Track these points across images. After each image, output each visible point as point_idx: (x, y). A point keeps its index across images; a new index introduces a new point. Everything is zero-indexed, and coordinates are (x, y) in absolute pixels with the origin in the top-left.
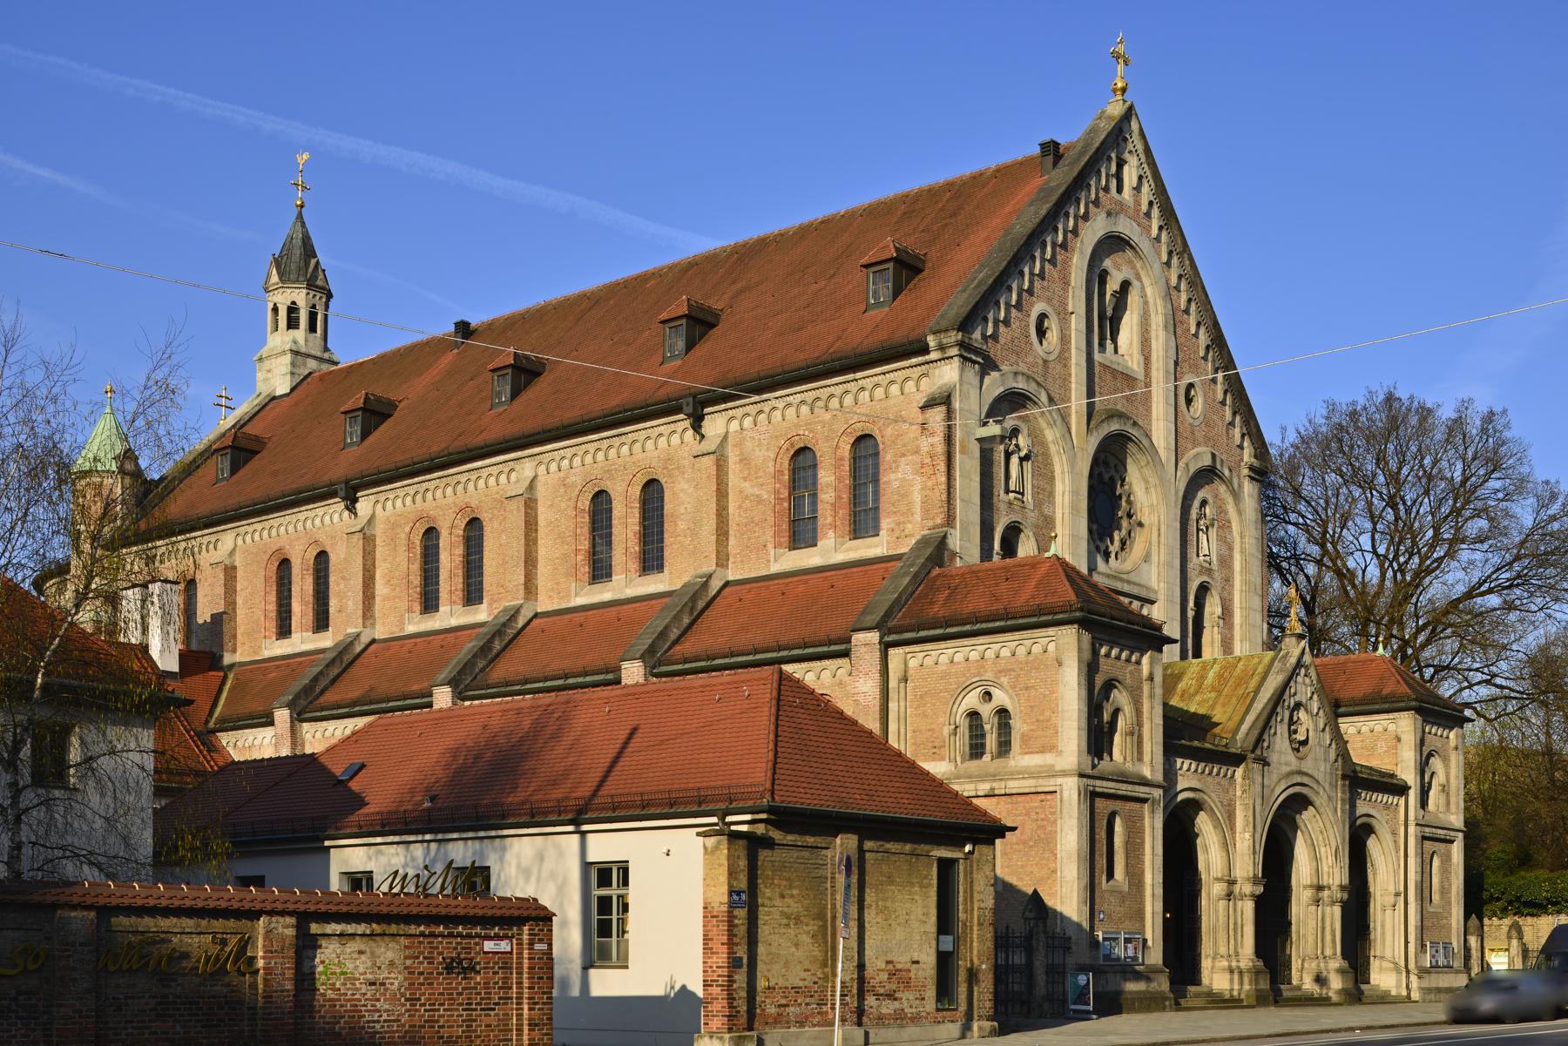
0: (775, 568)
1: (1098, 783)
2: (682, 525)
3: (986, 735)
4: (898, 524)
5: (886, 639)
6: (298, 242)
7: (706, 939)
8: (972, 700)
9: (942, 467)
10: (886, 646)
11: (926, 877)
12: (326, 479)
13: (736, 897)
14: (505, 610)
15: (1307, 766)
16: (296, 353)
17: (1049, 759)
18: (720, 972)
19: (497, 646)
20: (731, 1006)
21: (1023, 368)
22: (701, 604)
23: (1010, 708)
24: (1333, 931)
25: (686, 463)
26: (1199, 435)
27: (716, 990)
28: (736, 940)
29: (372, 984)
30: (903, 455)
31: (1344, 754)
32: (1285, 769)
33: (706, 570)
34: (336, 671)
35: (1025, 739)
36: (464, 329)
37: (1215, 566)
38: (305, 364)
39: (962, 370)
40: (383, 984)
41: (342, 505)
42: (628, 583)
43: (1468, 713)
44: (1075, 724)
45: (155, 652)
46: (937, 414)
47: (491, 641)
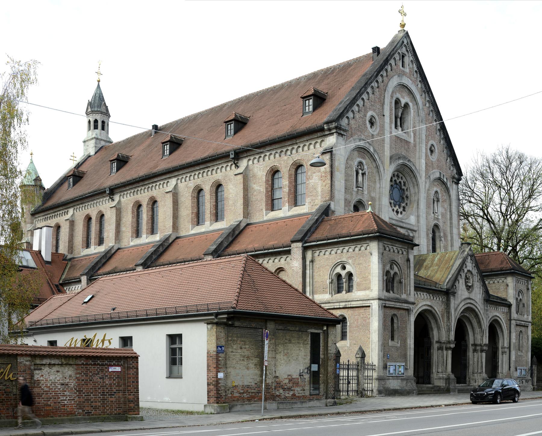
0: (265, 218)
1: (387, 302)
2: (231, 202)
3: (342, 282)
7: (208, 366)
8: (338, 270)
9: (329, 177)
10: (305, 249)
11: (306, 340)
12: (102, 187)
13: (220, 349)
14: (165, 236)
15: (472, 296)
16: (97, 139)
17: (367, 292)
18: (213, 379)
19: (161, 250)
20: (218, 393)
21: (363, 137)
22: (237, 232)
23: (352, 272)
24: (482, 363)
25: (232, 177)
26: (435, 166)
27: (212, 387)
28: (219, 366)
29: (62, 384)
30: (314, 173)
31: (486, 291)
32: (464, 297)
34: (104, 261)
35: (358, 284)
36: (155, 127)
37: (440, 217)
38: (100, 143)
39: (337, 139)
40: (68, 385)
41: (108, 198)
42: (211, 224)
43: (533, 275)
44: (377, 279)
45: (43, 254)
47: (158, 248)
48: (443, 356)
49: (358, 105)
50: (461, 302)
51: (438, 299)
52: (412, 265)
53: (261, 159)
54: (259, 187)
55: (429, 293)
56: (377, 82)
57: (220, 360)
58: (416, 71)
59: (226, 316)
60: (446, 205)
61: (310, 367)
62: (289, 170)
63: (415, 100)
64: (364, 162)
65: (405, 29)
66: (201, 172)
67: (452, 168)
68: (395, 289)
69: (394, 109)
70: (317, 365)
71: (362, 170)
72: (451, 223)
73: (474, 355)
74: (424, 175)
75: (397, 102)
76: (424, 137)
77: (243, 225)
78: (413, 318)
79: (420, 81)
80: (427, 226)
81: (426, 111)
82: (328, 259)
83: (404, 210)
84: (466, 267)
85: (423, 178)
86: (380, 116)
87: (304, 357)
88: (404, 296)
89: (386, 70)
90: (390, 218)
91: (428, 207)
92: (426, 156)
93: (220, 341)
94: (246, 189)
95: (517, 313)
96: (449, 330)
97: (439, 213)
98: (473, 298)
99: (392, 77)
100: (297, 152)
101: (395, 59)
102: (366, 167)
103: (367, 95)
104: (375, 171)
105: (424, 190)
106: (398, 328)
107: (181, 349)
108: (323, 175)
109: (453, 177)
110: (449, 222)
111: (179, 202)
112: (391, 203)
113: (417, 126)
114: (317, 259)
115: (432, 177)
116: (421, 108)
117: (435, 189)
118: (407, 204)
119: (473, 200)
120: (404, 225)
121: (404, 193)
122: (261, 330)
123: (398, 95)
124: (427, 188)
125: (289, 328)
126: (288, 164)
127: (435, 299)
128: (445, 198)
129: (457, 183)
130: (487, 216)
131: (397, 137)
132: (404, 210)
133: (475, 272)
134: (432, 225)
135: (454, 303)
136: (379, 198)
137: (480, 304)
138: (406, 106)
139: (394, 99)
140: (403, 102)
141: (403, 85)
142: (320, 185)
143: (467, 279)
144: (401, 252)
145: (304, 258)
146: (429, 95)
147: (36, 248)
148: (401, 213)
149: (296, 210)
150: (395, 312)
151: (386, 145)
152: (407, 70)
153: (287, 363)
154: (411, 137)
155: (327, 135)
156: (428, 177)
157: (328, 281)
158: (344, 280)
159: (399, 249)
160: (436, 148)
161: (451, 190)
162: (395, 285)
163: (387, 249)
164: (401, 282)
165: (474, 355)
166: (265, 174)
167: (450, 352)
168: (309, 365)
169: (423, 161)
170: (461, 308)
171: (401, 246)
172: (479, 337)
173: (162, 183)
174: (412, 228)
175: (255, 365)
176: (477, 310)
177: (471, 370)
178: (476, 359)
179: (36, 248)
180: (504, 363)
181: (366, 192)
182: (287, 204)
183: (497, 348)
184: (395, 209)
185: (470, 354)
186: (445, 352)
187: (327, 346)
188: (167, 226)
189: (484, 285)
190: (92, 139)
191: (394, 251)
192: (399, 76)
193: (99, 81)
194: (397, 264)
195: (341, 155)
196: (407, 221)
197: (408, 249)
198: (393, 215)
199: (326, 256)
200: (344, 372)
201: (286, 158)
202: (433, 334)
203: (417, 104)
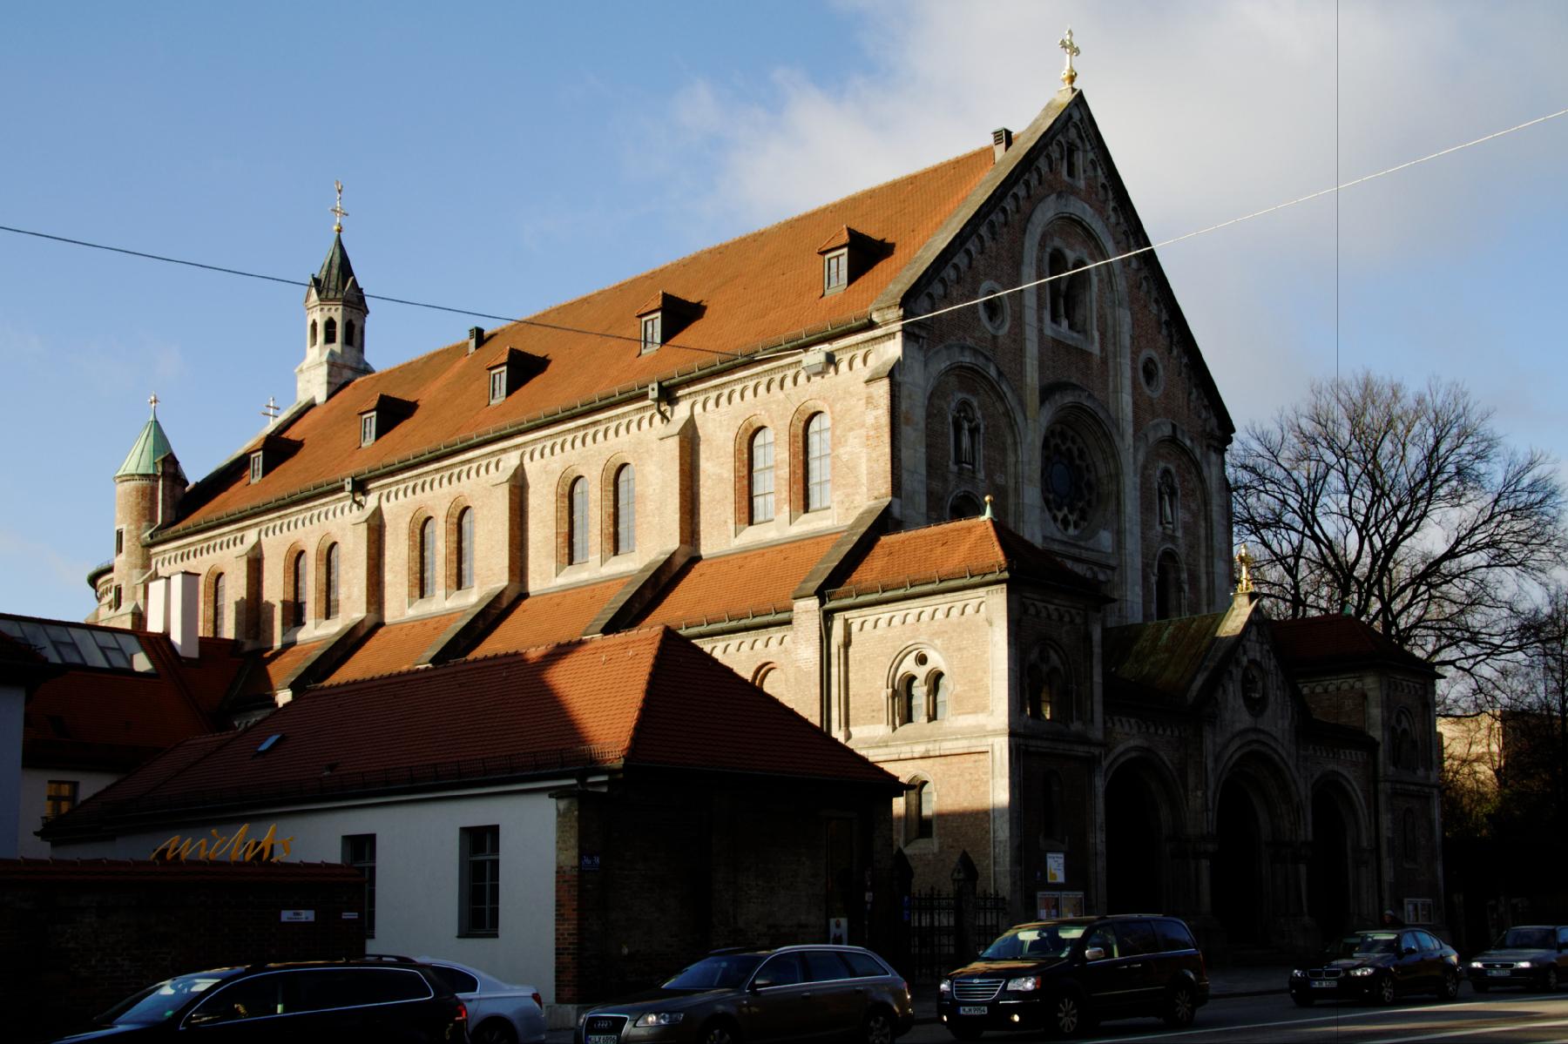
1: (1033, 742)
2: (651, 506)
4: (848, 495)
5: (829, 606)
6: (337, 260)
7: (559, 905)
8: (909, 665)
10: (828, 616)
21: (970, 342)
25: (654, 446)
30: (851, 429)
32: (1239, 726)
35: (959, 700)
37: (1179, 534)
49: (956, 267)
50: (1233, 737)
52: (1097, 650)
58: (1103, 186)
59: (604, 778)
65: (1075, 85)
71: (970, 421)
72: (1210, 548)
74: (1130, 431)
76: (1126, 340)
78: (1100, 783)
80: (1144, 556)
83: (1083, 517)
84: (1245, 653)
85: (1129, 439)
90: (1045, 538)
91: (1146, 507)
95: (1395, 765)
99: (1041, 200)
101: (1049, 157)
102: (979, 414)
107: (496, 864)
110: (1203, 545)
117: (1162, 465)
118: (1089, 503)
120: (1085, 554)
123: (1057, 242)
124: (1140, 463)
129: (1222, 451)
130: (1311, 529)
131: (1058, 342)
133: (1271, 664)
136: (1016, 489)
139: (1049, 250)
142: (864, 460)
144: (1067, 619)
149: (807, 525)
154: (1093, 343)
159: (1028, 602)
163: (1032, 611)
169: (1127, 399)
179: (154, 625)
184: (1060, 515)
189: (1296, 695)
191: (1049, 616)
196: (1090, 544)
198: (1055, 530)
199: (879, 632)
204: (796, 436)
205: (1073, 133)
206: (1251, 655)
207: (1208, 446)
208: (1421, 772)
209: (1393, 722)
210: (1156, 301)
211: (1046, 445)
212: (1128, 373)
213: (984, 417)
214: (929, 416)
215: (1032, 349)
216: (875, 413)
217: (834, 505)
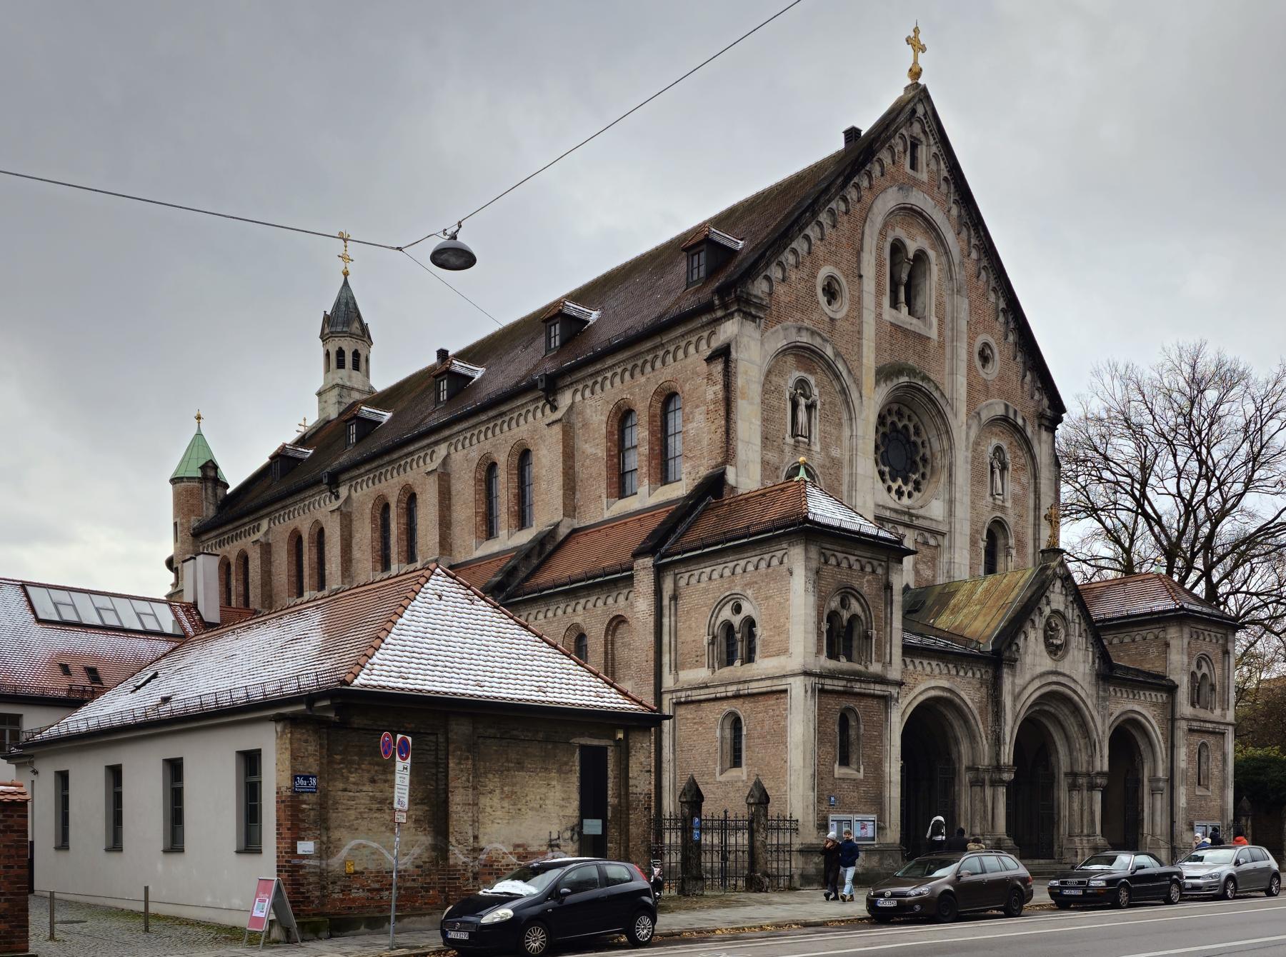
0: (607, 515)
1: (828, 681)
2: (544, 486)
3: (736, 642)
8: (726, 613)
9: (722, 412)
11: (566, 764)
13: (301, 782)
15: (1064, 667)
16: (343, 387)
21: (807, 323)
22: (549, 548)
23: (754, 617)
24: (1092, 813)
30: (697, 406)
32: (1039, 670)
33: (556, 519)
37: (1009, 504)
42: (510, 536)
45: (201, 607)
46: (718, 367)
48: (983, 800)
49: (794, 251)
51: (970, 674)
53: (598, 387)
54: (594, 448)
55: (946, 662)
56: (845, 200)
57: (303, 811)
58: (945, 179)
60: (1025, 478)
61: (581, 825)
62: (650, 406)
63: (943, 245)
64: (812, 380)
66: (491, 425)
67: (1037, 397)
68: (855, 653)
69: (888, 262)
70: (599, 822)
73: (1070, 797)
75: (897, 248)
76: (963, 326)
77: (563, 531)
79: (955, 202)
80: (973, 523)
81: (971, 267)
82: (706, 590)
83: (917, 489)
84: (1048, 603)
86: (851, 278)
87: (562, 803)
88: (875, 668)
89: (869, 175)
91: (977, 479)
92: (970, 367)
93: (303, 763)
94: (569, 455)
95: (1193, 705)
96: (997, 741)
97: (1008, 495)
98: (1067, 672)
100: (664, 363)
102: (816, 391)
103: (817, 229)
104: (839, 399)
105: (964, 444)
106: (858, 738)
108: (711, 407)
109: (1041, 416)
110: (1031, 514)
111: (454, 493)
112: (882, 474)
113: (948, 303)
114: (684, 591)
115: (985, 416)
116: (957, 261)
117: (995, 442)
118: (923, 476)
119: (1107, 475)
121: (917, 452)
122: (432, 738)
123: (899, 232)
124: (971, 440)
125: (515, 733)
126: (647, 392)
127: (962, 673)
128: (1023, 461)
129: (1052, 430)
132: (917, 489)
134: (989, 521)
135: (1013, 683)
136: (851, 461)
137: (1086, 686)
138: (921, 256)
139: (890, 240)
140: (912, 247)
141: (911, 209)
143: (1052, 629)
144: (868, 569)
145: (658, 592)
146: (977, 231)
147: (188, 598)
148: (910, 495)
150: (851, 703)
151: (865, 342)
152: (923, 176)
153: (513, 817)
154: (930, 326)
155: (721, 318)
156: (974, 413)
157: (706, 640)
158: (739, 636)
159: (828, 553)
160: (996, 351)
161: (1035, 444)
162: (855, 643)
164: (868, 637)
165: (1070, 797)
166: (605, 419)
167: (1002, 791)
168: (575, 821)
169: (962, 381)
170: (1032, 693)
171: (868, 555)
172: (1083, 757)
173: (422, 454)
174: (934, 526)
175: (416, 821)
176: (1076, 698)
177: (1064, 828)
178: (1076, 806)
180: (1158, 813)
181: (816, 447)
182: (646, 481)
183: (1138, 782)
184: (895, 486)
185: (1063, 794)
186: (988, 791)
187: (627, 778)
188: (430, 544)
190: (333, 387)
191: (850, 567)
192: (900, 188)
193: (346, 274)
194: (859, 596)
195: (752, 362)
197: (887, 562)
199: (702, 585)
200: (673, 835)
201: (643, 379)
202: (959, 752)
203: (947, 252)
204: (654, 416)
205: (916, 128)
206: (1054, 606)
207: (1040, 426)
208: (1218, 712)
209: (1194, 668)
210: (994, 290)
211: (881, 419)
212: (963, 354)
213: (821, 395)
214: (765, 392)
215: (869, 330)
216: (714, 388)
217: (683, 477)
